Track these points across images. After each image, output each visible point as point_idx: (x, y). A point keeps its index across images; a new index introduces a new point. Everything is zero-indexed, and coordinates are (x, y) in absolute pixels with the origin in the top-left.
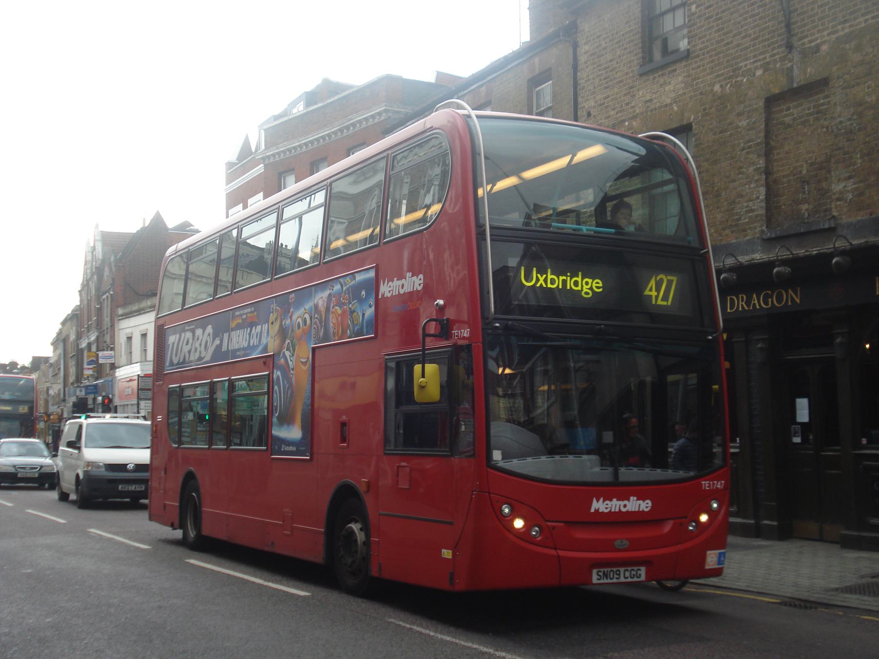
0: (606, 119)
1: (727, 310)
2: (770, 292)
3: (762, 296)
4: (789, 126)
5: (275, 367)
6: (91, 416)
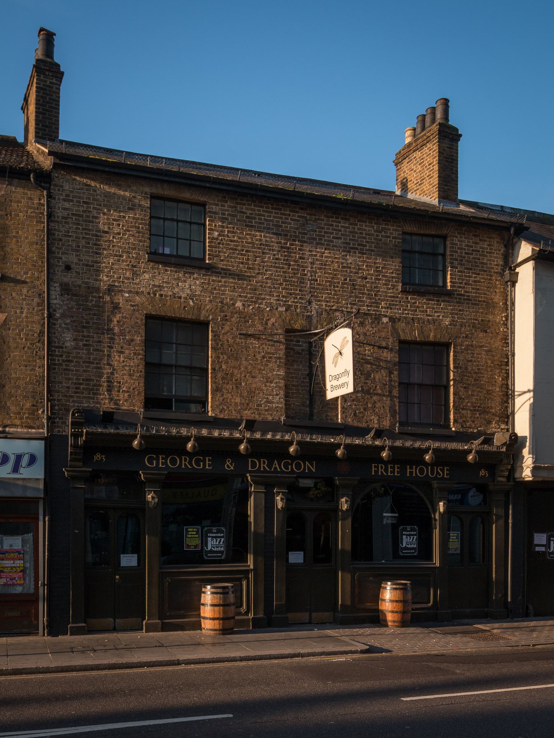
0: (277, 243)
1: (206, 467)
2: (155, 456)
3: (146, 459)
4: (299, 353)
5: (165, 245)
6: (8, 437)
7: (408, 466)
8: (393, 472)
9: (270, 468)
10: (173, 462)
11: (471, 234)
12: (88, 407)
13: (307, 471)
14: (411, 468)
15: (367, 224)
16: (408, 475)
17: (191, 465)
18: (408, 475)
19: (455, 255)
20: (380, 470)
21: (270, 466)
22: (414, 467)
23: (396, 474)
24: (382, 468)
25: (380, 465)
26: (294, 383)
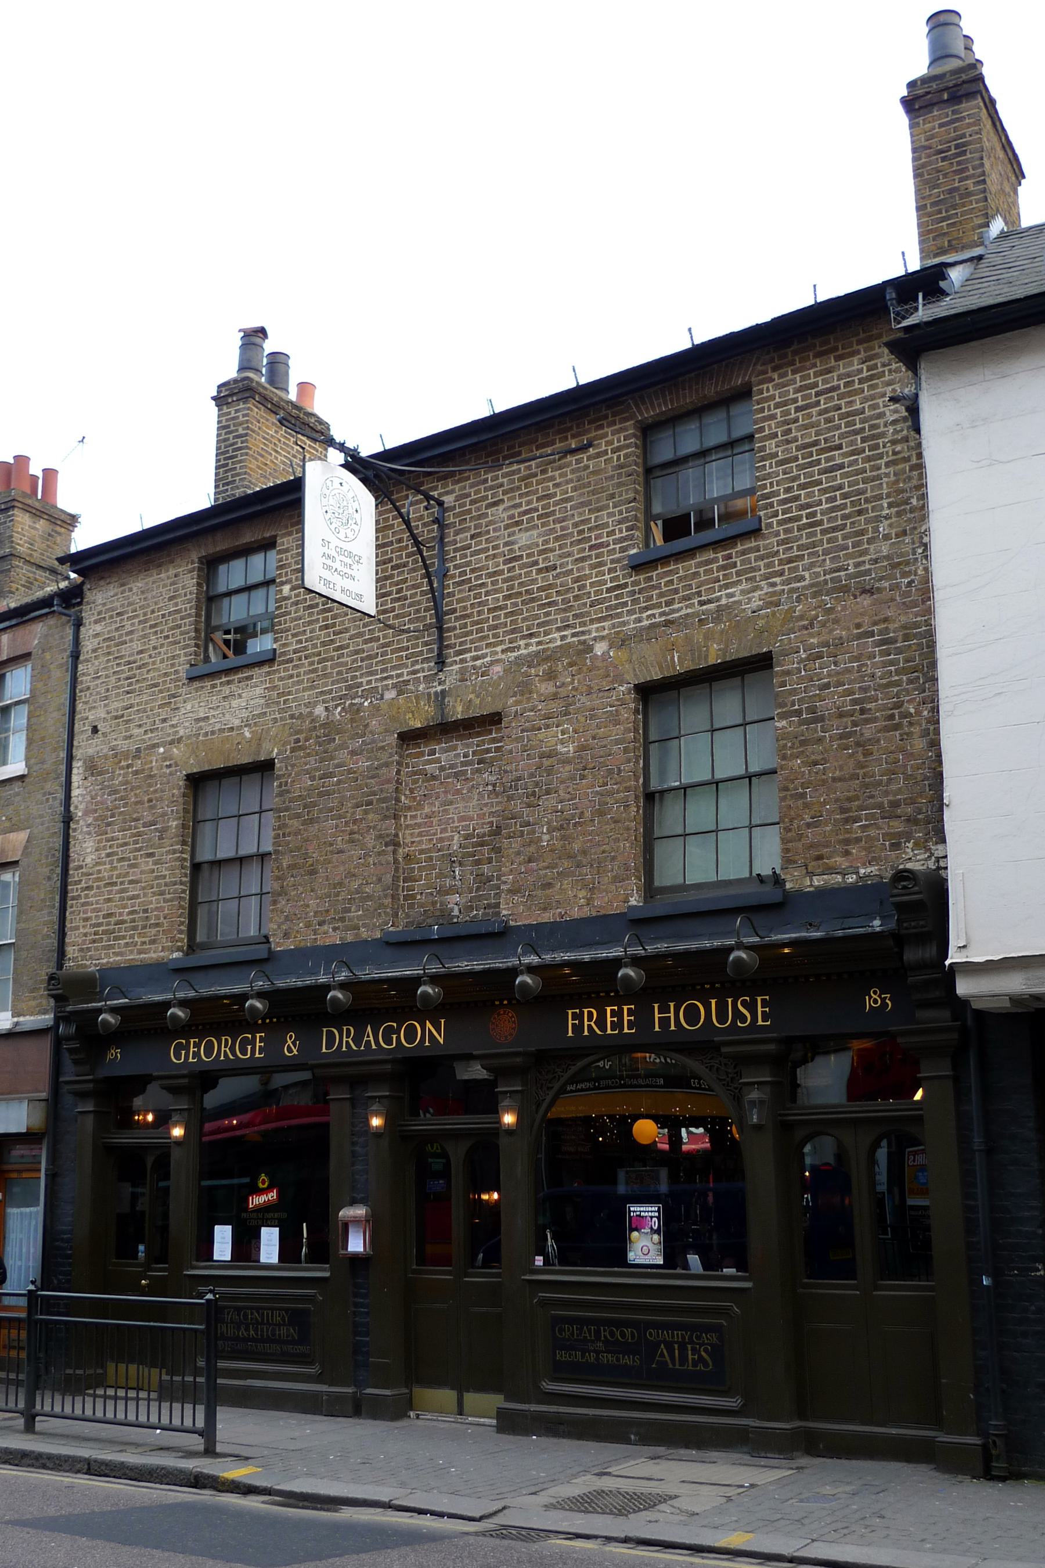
3: (702, 1020)
4: (434, 778)
7: (656, 1006)
8: (618, 1025)
9: (358, 1045)
10: (209, 1051)
11: (811, 354)
12: (108, 963)
13: (427, 1044)
14: (664, 1009)
15: (862, 336)
16: (657, 1029)
17: (234, 1054)
18: (657, 1029)
19: (769, 425)
20: (586, 1023)
21: (357, 1041)
22: (672, 1005)
23: (626, 1031)
24: (590, 1019)
25: (586, 1011)
26: (424, 847)
